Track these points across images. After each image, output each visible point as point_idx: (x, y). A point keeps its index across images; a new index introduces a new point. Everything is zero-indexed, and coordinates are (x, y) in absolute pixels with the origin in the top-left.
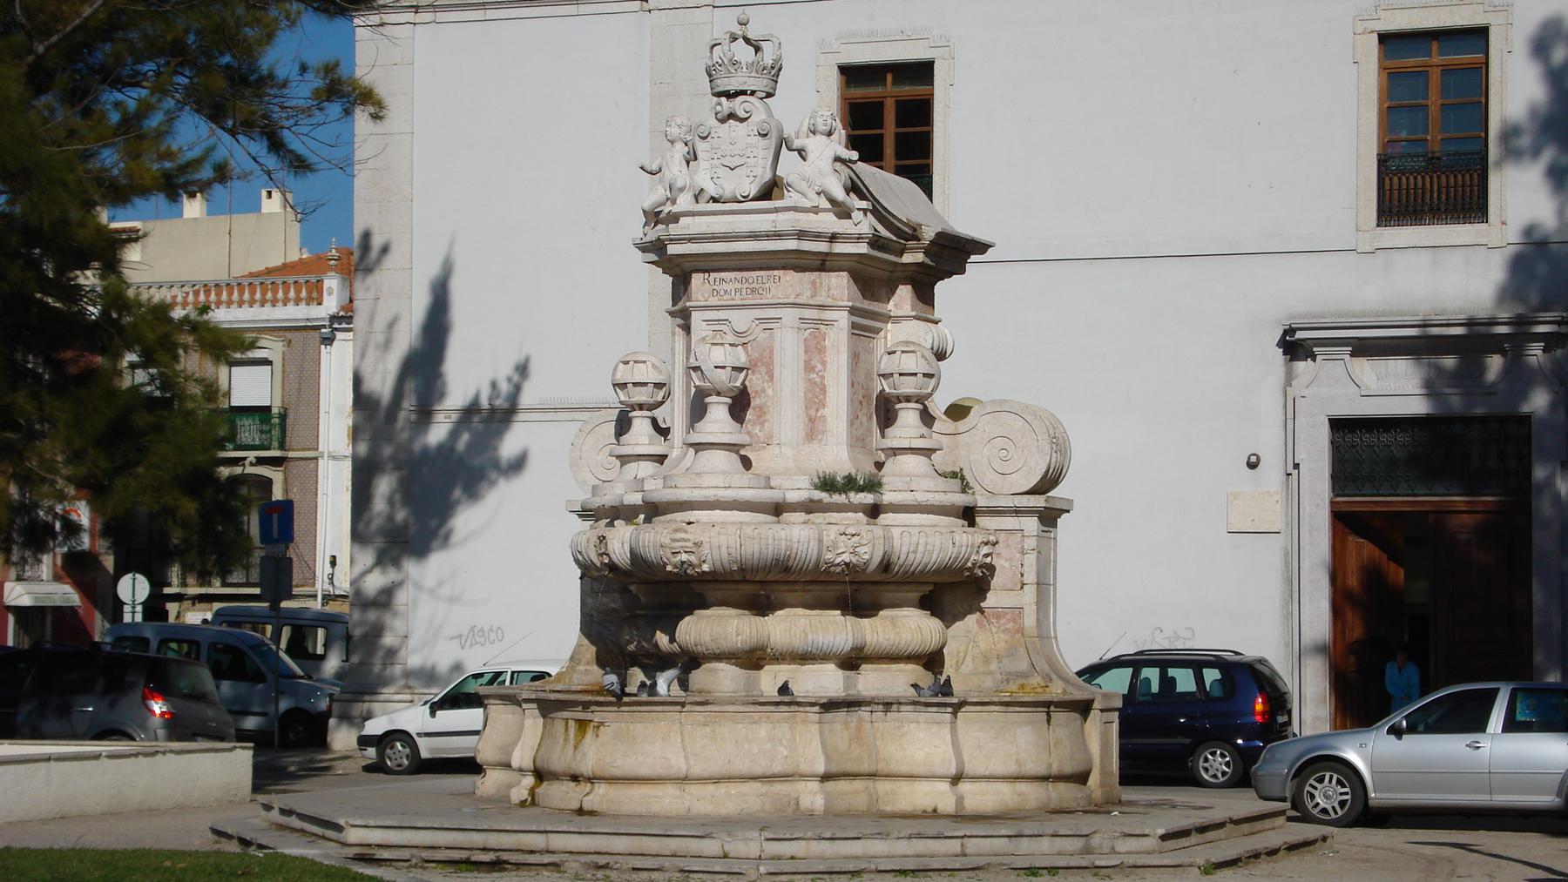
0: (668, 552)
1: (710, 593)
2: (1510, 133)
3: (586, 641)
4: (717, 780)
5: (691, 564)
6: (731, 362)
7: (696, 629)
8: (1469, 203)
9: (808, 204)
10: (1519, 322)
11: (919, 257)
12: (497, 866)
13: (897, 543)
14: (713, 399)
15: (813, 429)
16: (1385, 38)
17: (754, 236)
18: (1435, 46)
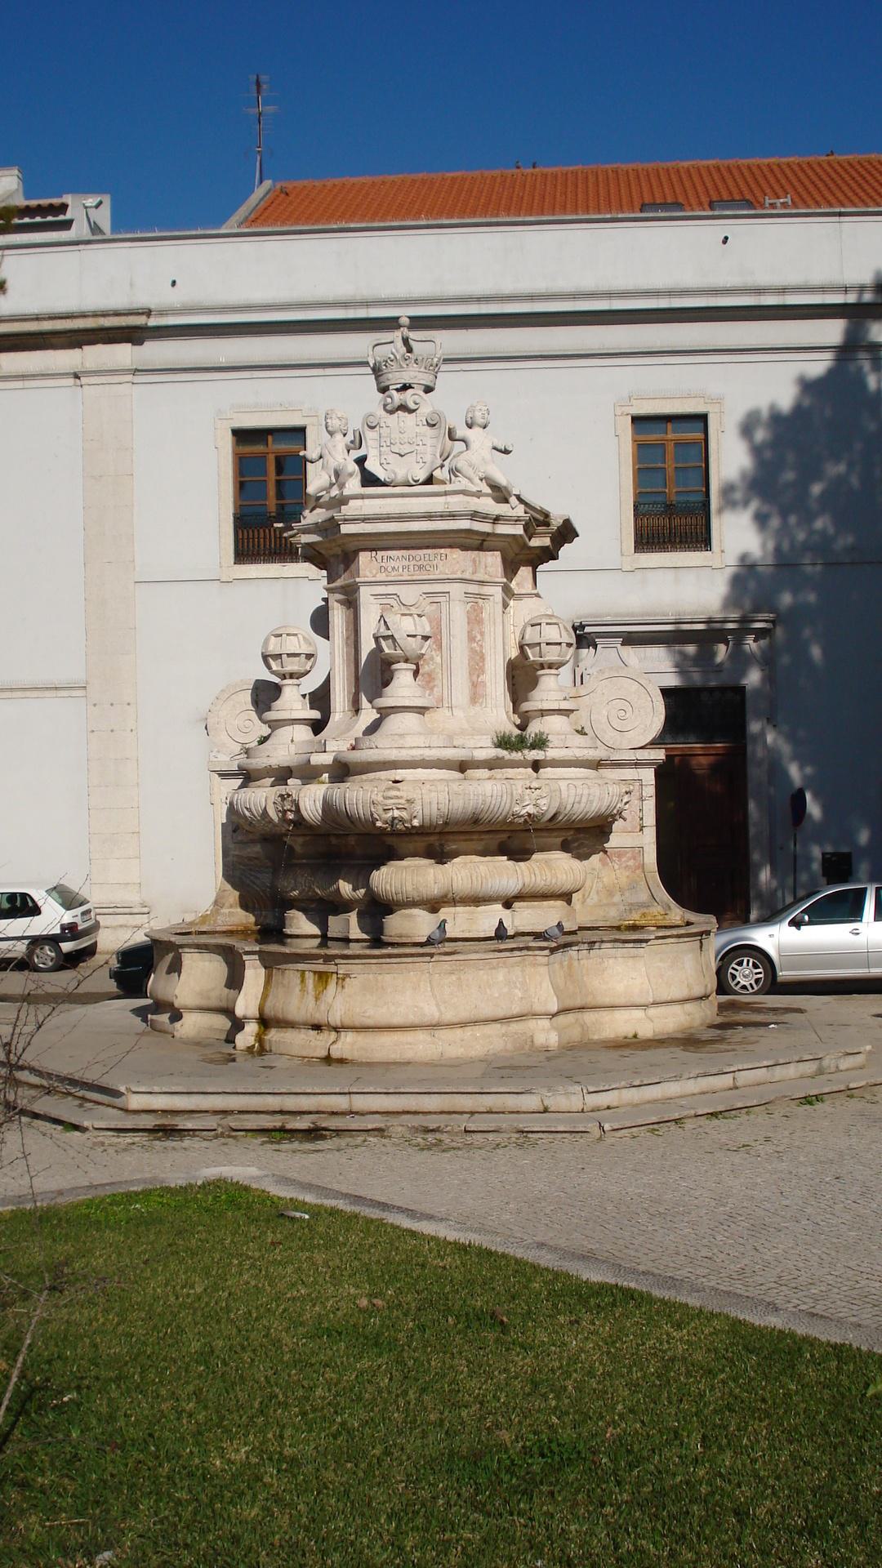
0: (380, 808)
1: (54, 341)
2: (728, 490)
3: (228, 887)
4: (463, 1024)
5: (402, 820)
6: (420, 632)
7: (389, 878)
8: (701, 539)
9: (474, 489)
10: (744, 620)
12: (314, 1134)
13: (564, 794)
14: (402, 665)
15: (476, 694)
16: (636, 420)
17: (429, 517)
18: (670, 426)
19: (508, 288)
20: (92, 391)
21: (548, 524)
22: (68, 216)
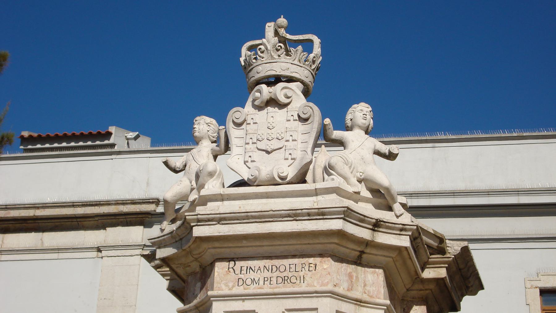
1: (86, 223)
9: (351, 189)
11: (442, 273)
17: (294, 215)
19: (435, 187)
20: (108, 262)
21: (442, 251)
22: (112, 141)
